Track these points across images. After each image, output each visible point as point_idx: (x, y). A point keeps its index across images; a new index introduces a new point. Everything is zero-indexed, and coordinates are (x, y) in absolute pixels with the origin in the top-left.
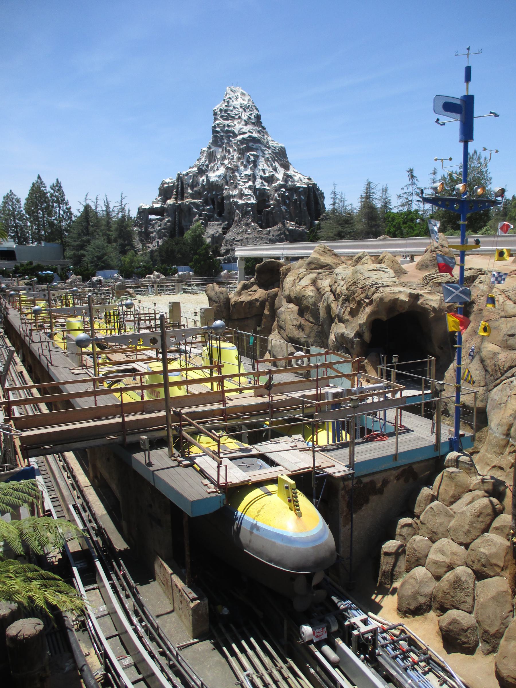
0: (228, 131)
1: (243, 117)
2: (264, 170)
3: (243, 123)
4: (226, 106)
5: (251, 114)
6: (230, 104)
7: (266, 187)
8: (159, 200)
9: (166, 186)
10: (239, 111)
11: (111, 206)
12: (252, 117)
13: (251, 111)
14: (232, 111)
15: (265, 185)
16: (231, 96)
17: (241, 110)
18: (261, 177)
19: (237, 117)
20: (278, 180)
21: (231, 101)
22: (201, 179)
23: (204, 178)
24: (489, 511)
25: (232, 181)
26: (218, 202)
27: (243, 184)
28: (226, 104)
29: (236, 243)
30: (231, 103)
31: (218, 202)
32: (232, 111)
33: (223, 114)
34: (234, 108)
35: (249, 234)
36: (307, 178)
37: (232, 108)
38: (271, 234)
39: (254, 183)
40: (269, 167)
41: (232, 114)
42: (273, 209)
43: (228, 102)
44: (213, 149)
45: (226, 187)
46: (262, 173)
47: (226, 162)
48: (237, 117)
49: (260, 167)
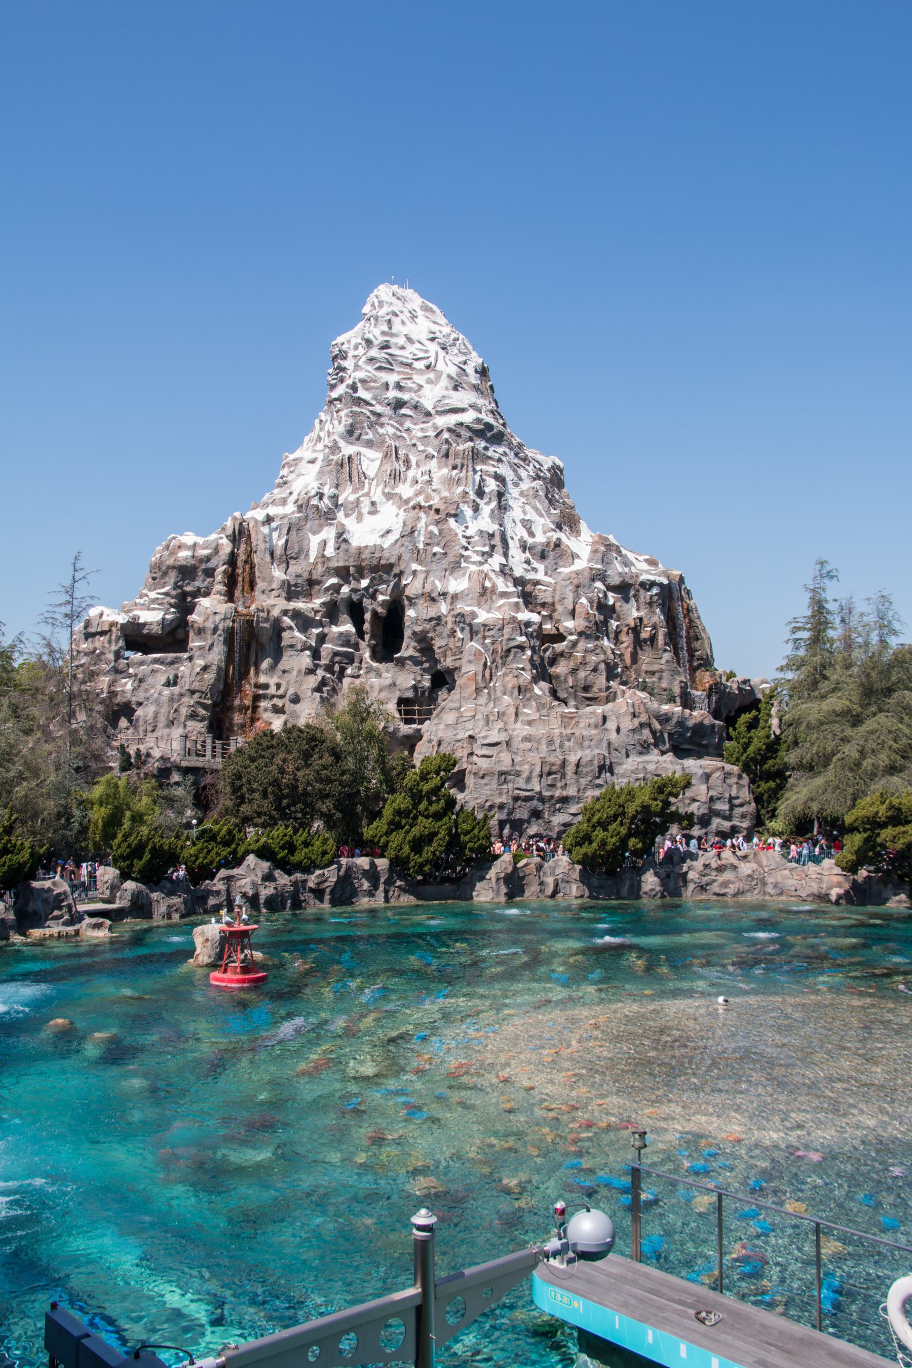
0: (399, 404)
1: (440, 366)
2: (527, 525)
3: (444, 382)
4: (383, 333)
5: (465, 363)
6: (394, 330)
7: (540, 576)
8: (154, 601)
9: (184, 554)
10: (427, 351)
11: (454, 375)
12: (470, 369)
13: (465, 354)
14: (403, 348)
15: (535, 570)
16: (396, 309)
17: (433, 347)
18: (524, 547)
19: (420, 365)
20: (574, 556)
21: (396, 321)
22: (314, 541)
23: (329, 533)
24: (688, 1258)
25: (436, 549)
26: (375, 613)
27: (479, 558)
28: (385, 328)
29: (485, 751)
30: (397, 327)
31: (375, 613)
32: (403, 348)
33: (374, 352)
34: (409, 340)
35: (530, 723)
36: (646, 561)
37: (401, 341)
38: (611, 725)
39: (506, 555)
40: (541, 515)
41: (406, 355)
42: (574, 644)
43: (389, 322)
44: (348, 450)
45: (415, 566)
46: (521, 532)
47: (406, 490)
48: (420, 365)
49: (517, 510)
